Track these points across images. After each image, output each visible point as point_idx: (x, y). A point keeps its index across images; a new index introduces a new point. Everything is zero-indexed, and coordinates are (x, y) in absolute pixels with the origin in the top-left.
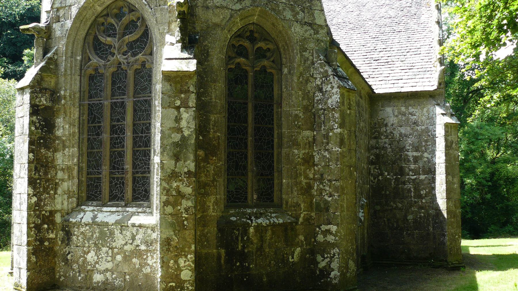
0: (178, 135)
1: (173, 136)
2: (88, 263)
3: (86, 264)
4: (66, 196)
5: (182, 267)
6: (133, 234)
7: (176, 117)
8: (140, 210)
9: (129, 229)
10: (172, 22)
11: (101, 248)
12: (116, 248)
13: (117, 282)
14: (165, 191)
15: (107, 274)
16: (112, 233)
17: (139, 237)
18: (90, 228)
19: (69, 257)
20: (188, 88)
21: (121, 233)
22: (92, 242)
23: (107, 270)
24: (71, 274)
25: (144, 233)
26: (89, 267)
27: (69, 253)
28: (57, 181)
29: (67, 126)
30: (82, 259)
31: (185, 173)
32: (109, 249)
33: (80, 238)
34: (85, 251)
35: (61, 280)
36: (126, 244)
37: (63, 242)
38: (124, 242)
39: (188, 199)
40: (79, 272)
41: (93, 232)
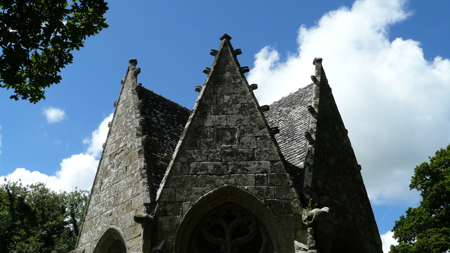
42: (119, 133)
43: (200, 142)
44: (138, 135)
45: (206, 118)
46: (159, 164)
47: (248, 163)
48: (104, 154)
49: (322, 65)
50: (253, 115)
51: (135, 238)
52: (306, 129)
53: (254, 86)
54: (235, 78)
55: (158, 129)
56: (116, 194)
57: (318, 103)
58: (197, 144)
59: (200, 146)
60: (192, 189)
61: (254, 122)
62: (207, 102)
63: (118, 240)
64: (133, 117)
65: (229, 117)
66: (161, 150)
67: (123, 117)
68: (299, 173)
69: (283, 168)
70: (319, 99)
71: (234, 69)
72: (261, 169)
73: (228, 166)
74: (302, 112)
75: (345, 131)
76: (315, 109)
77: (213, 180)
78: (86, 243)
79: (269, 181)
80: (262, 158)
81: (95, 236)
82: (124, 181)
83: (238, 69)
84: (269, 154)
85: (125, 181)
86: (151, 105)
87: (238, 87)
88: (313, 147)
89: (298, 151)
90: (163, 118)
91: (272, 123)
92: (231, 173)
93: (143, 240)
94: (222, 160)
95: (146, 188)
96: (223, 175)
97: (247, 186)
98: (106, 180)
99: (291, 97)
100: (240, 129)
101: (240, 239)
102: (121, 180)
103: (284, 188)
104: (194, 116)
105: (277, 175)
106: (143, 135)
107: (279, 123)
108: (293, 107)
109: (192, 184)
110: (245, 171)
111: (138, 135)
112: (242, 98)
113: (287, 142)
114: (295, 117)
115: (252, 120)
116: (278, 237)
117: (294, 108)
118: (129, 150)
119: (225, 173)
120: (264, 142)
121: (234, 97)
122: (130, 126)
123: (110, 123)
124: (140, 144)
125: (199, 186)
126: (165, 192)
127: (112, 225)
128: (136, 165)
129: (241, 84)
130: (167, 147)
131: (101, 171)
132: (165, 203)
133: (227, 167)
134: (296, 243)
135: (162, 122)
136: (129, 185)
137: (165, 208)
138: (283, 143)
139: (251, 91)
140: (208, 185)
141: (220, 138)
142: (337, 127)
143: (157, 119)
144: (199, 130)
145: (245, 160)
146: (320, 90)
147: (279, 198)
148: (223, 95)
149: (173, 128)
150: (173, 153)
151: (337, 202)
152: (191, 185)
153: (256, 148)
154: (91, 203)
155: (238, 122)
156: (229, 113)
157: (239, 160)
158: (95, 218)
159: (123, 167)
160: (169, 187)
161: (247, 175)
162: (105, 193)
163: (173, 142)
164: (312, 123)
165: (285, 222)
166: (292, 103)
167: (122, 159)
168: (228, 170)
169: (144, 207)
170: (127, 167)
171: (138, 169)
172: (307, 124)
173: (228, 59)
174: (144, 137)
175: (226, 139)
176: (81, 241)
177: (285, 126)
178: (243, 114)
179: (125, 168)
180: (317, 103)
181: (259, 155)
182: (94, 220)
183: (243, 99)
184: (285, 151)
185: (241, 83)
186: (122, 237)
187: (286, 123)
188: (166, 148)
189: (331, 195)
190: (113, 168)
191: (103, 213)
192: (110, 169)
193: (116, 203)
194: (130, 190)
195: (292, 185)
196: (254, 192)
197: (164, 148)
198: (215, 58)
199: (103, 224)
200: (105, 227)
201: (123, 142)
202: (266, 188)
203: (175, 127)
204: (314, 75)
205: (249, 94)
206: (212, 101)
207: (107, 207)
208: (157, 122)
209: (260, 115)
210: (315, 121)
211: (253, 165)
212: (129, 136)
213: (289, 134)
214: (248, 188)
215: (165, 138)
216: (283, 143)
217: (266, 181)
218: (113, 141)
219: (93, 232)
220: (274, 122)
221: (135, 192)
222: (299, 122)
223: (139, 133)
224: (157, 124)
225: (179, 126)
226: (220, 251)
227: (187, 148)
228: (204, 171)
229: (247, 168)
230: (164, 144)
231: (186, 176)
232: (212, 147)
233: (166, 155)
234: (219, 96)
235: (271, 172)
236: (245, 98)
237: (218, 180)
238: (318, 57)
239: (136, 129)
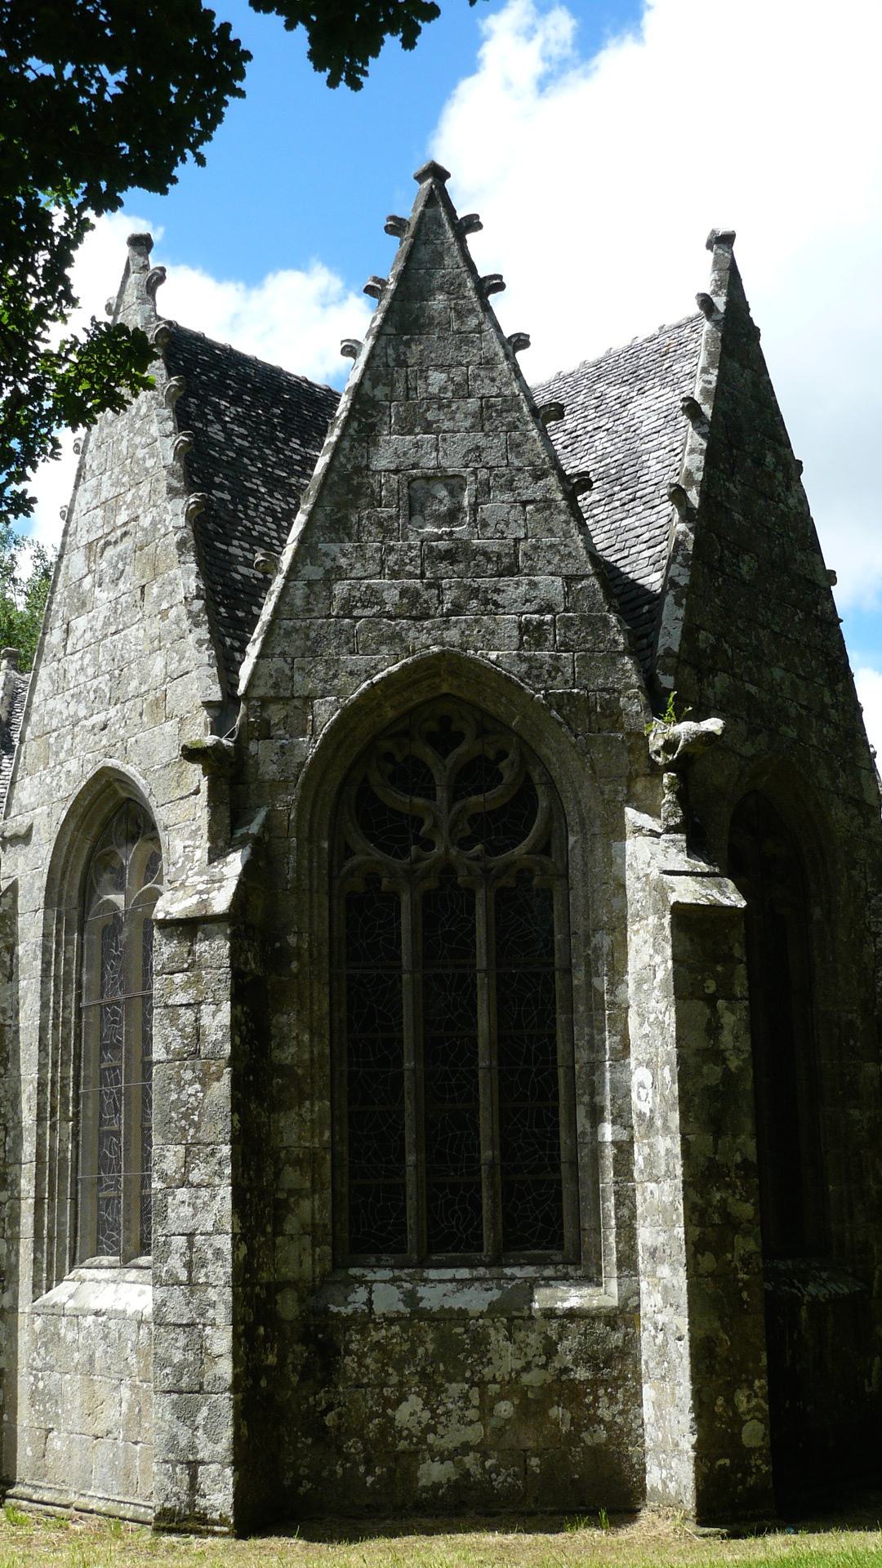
0: (716, 1068)
1: (705, 1069)
2: (400, 1432)
3: (394, 1437)
4: (307, 1240)
5: (743, 1413)
6: (547, 1338)
7: (709, 1022)
8: (549, 1272)
9: (536, 1327)
10: (637, 776)
11: (442, 1385)
12: (494, 1381)
13: (501, 1479)
14: (697, 1213)
15: (466, 1459)
16: (480, 1341)
17: (568, 1346)
18: (404, 1330)
19: (330, 1419)
20: (731, 949)
21: (509, 1338)
22: (413, 1369)
23: (466, 1448)
24: (339, 1470)
25: (585, 1334)
26: (403, 1445)
27: (330, 1407)
28: (282, 1196)
29: (306, 1037)
30: (376, 1421)
31: (737, 1166)
32: (471, 1387)
33: (368, 1361)
34: (387, 1400)
35: (302, 1490)
36: (527, 1368)
37: (305, 1375)
38: (519, 1364)
39: (746, 1234)
40: (368, 1461)
41: (416, 1341)
42: (110, 477)
43: (360, 519)
44: (172, 492)
45: (376, 444)
46: (239, 577)
47: (499, 582)
48: (68, 539)
49: (732, 254)
50: (515, 434)
51: (182, 798)
52: (673, 467)
53: (519, 340)
54: (461, 315)
55: (227, 462)
56: (116, 666)
57: (714, 384)
58: (352, 527)
59: (359, 532)
60: (338, 660)
61: (519, 455)
62: (380, 392)
63: (129, 799)
64: (154, 429)
65: (444, 440)
66: (241, 532)
67: (119, 426)
68: (647, 607)
69: (601, 597)
70: (716, 372)
71: (460, 285)
72: (538, 601)
73: (441, 591)
74: (665, 408)
75: (793, 466)
76: (702, 406)
77: (399, 635)
78: (35, 806)
79: (558, 638)
80: (540, 569)
81: (61, 786)
82: (138, 630)
83: (470, 284)
84: (562, 556)
85: (142, 631)
86: (202, 382)
87: (467, 342)
88: (690, 529)
89: (646, 537)
90: (242, 424)
91: (574, 434)
92: (450, 613)
93: (207, 809)
94: (425, 574)
95: (206, 655)
96: (428, 617)
97: (496, 653)
98: (80, 623)
99: (633, 351)
100: (476, 479)
101: (474, 798)
102: (129, 627)
103: (604, 657)
104: (341, 438)
105: (582, 618)
106: (189, 492)
107: (596, 438)
108: (640, 387)
109: (339, 646)
110: (491, 604)
111: (172, 492)
112: (482, 381)
113: (617, 504)
114: (644, 424)
115: (511, 448)
116: (580, 794)
117: (641, 392)
118: (146, 535)
119: (432, 612)
120: (546, 520)
121: (457, 375)
122: (144, 459)
123: (78, 442)
124: (182, 521)
125: (360, 652)
126: (264, 670)
127: (111, 757)
128: (171, 584)
129: (479, 333)
130: (259, 520)
131: (62, 594)
132: (265, 702)
133: (439, 596)
134: (631, 814)
135: (238, 437)
136: (156, 642)
137: (265, 715)
138: (605, 505)
139: (509, 357)
140: (384, 649)
141: (417, 506)
142: (770, 459)
143: (224, 429)
144: (355, 482)
145: (489, 572)
146: (723, 340)
147: (585, 688)
148: (427, 371)
149: (272, 455)
150: (280, 553)
151: (753, 689)
152: (335, 647)
153: (523, 536)
154: (37, 688)
155: (471, 456)
156: (444, 427)
157: (473, 573)
158: (55, 734)
159: (132, 588)
160: (273, 655)
161: (495, 619)
162: (80, 662)
163: (274, 501)
164: (692, 451)
165: (601, 755)
166: (635, 372)
167: (128, 560)
168: (441, 602)
169: (205, 712)
170: (144, 587)
171: (180, 597)
172: (676, 452)
173: (440, 249)
174: (192, 500)
175: (435, 510)
176: (19, 799)
177: (612, 448)
178: (487, 430)
179: (139, 592)
180: (709, 386)
181: (531, 559)
182: (52, 740)
183: (487, 381)
184: (609, 531)
185: (479, 330)
186: (143, 796)
187: (617, 440)
188: (254, 523)
189: (737, 671)
190: (100, 586)
191: (79, 720)
192: (90, 589)
193: (118, 693)
194: (159, 658)
195: (625, 648)
196: (515, 670)
197: (249, 524)
198: (401, 244)
199: (83, 753)
200: (89, 761)
201: (125, 507)
202: (551, 656)
203: (278, 451)
204: (707, 289)
205: (505, 365)
206: (392, 391)
207: (90, 704)
208: (223, 440)
209: (535, 433)
210: (701, 444)
211: (513, 590)
212: (144, 490)
213: (624, 479)
214: (498, 657)
215: (251, 489)
216: (605, 505)
217: (551, 637)
218: (95, 501)
219: (54, 774)
220: (579, 433)
221: (173, 667)
222: (655, 442)
223: (176, 484)
224: (224, 446)
225: (291, 444)
226: (421, 834)
227: (322, 539)
228: (372, 608)
229: (496, 597)
230: (249, 512)
231: (320, 621)
232: (395, 534)
233: (262, 558)
234: (413, 371)
235: (566, 610)
236: (493, 380)
237: (412, 634)
238: (723, 229)
239: (165, 472)
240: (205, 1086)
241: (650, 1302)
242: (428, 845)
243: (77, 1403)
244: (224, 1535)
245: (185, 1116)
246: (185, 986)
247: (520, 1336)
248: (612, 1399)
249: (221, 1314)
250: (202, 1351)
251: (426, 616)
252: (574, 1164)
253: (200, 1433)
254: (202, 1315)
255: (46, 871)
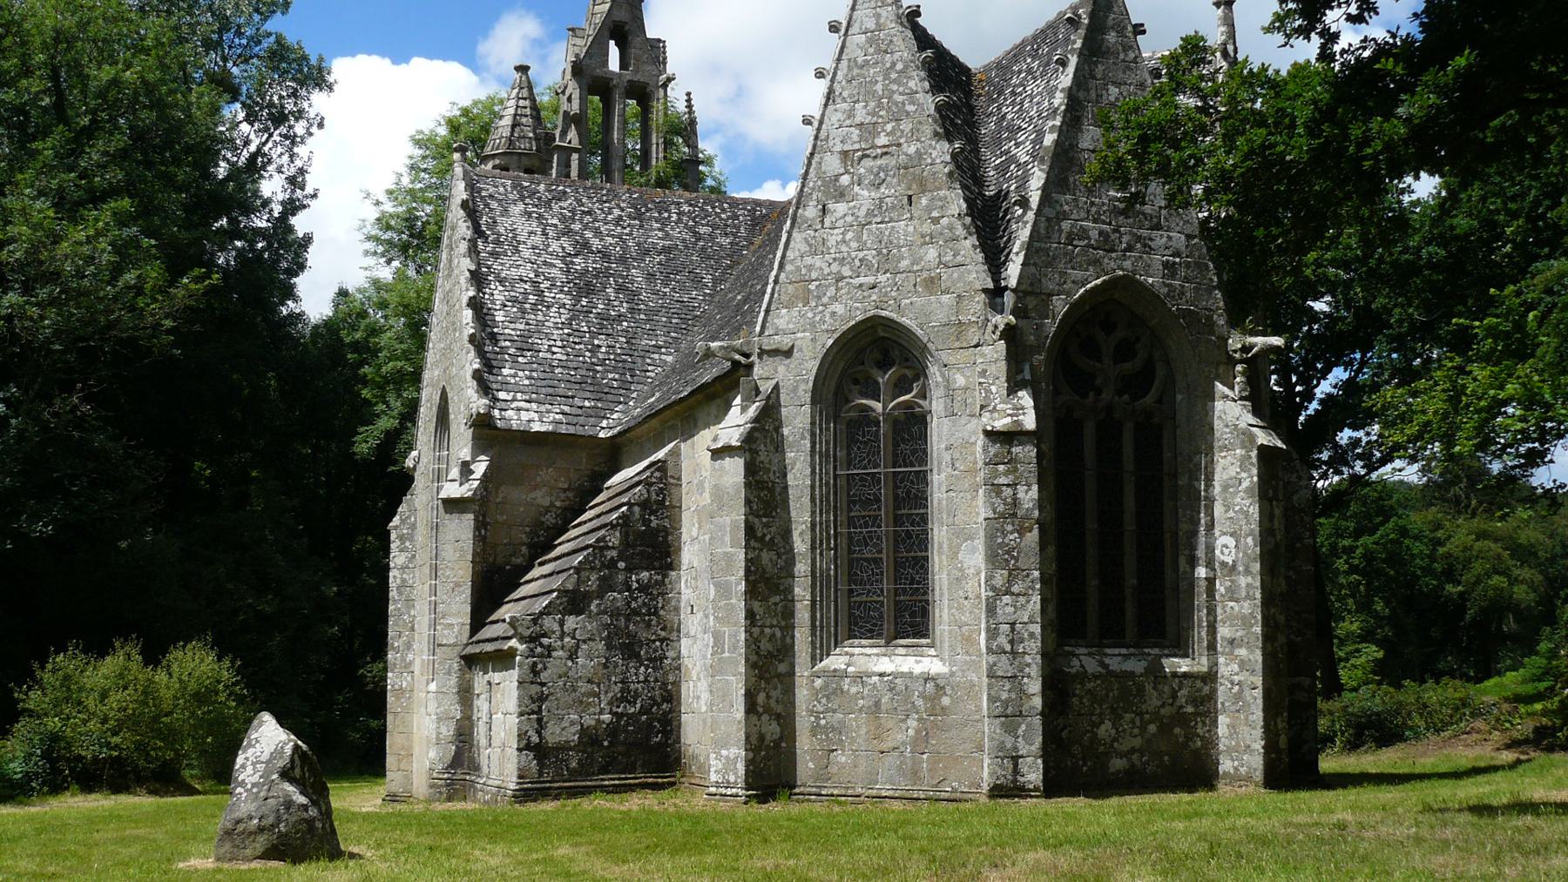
8: (1166, 652)
12: (1147, 713)
16: (1141, 690)
18: (1103, 683)
19: (1064, 734)
23: (1133, 751)
26: (1102, 748)
27: (1065, 728)
36: (1163, 706)
38: (1159, 703)
40: (1084, 759)
45: (1081, 131)
62: (1081, 95)
92: (1125, 250)
134: (1219, 386)
140: (1091, 268)
211: (1160, 240)
237: (1106, 260)
240: (1021, 535)
241: (1227, 668)
242: (1099, 392)
243: (863, 731)
244: (1037, 797)
245: (1008, 552)
246: (1006, 474)
247: (1160, 687)
248: (1204, 724)
249: (1035, 671)
250: (1022, 693)
251: (1113, 250)
252: (1176, 589)
253: (1020, 739)
254: (1021, 671)
255: (812, 378)
